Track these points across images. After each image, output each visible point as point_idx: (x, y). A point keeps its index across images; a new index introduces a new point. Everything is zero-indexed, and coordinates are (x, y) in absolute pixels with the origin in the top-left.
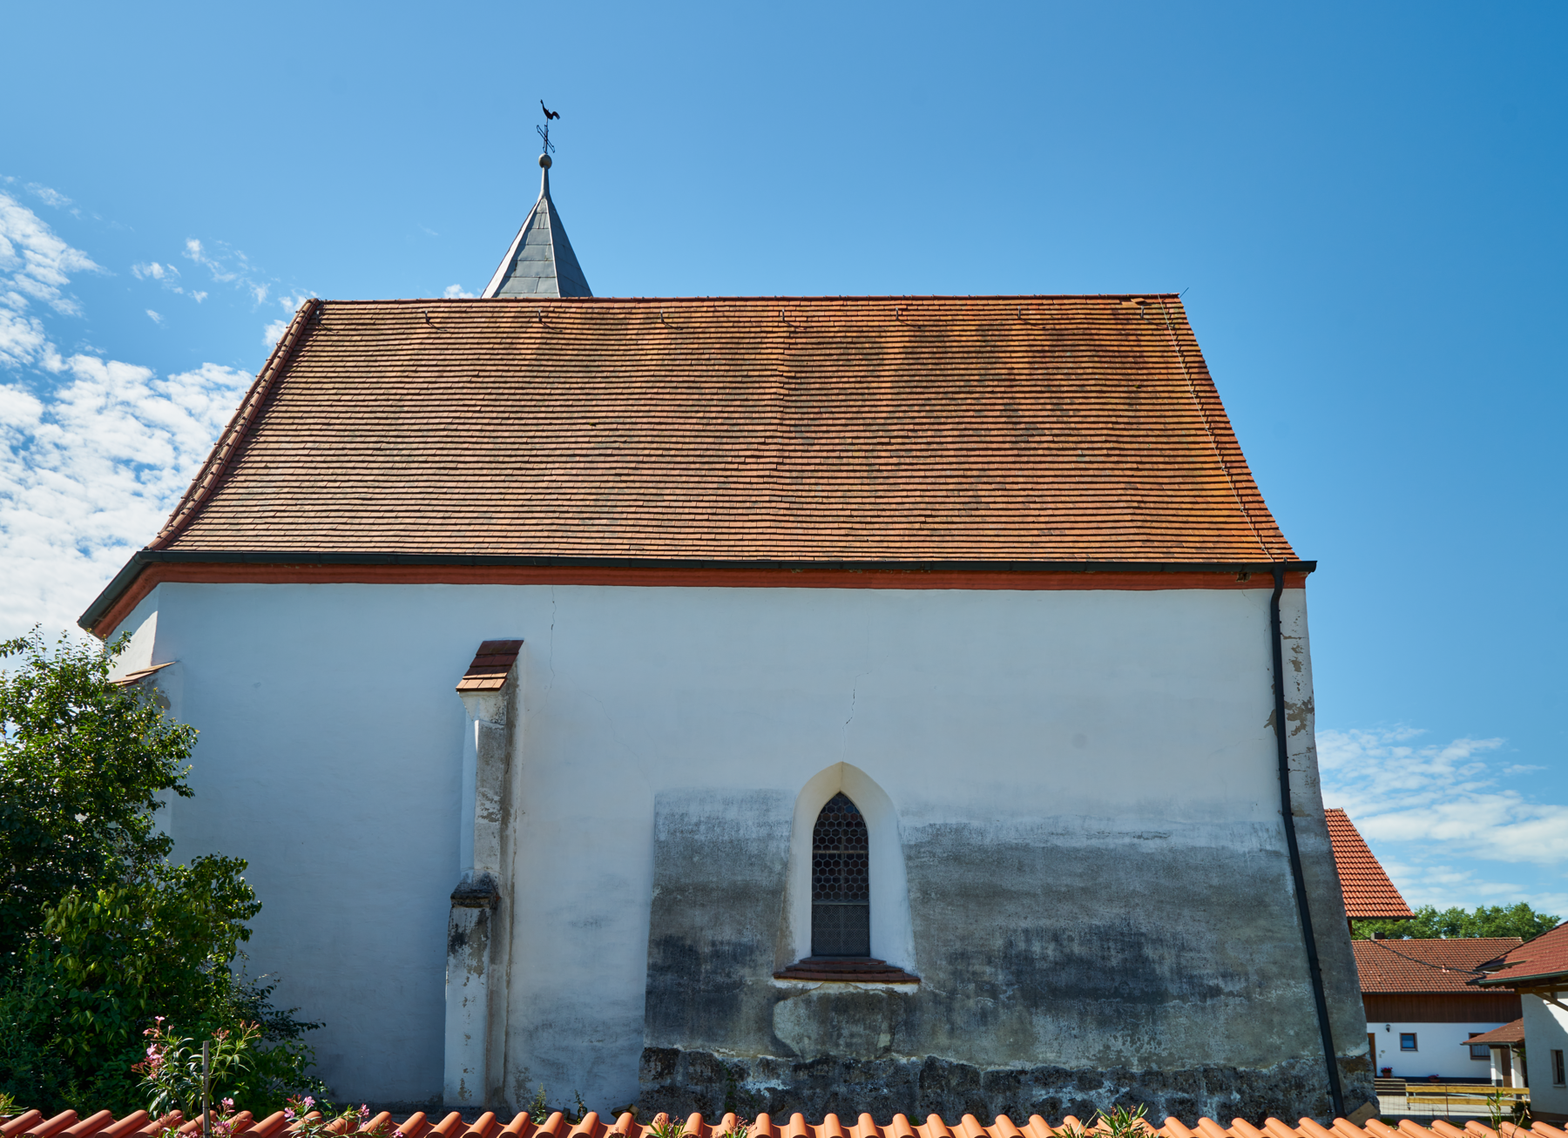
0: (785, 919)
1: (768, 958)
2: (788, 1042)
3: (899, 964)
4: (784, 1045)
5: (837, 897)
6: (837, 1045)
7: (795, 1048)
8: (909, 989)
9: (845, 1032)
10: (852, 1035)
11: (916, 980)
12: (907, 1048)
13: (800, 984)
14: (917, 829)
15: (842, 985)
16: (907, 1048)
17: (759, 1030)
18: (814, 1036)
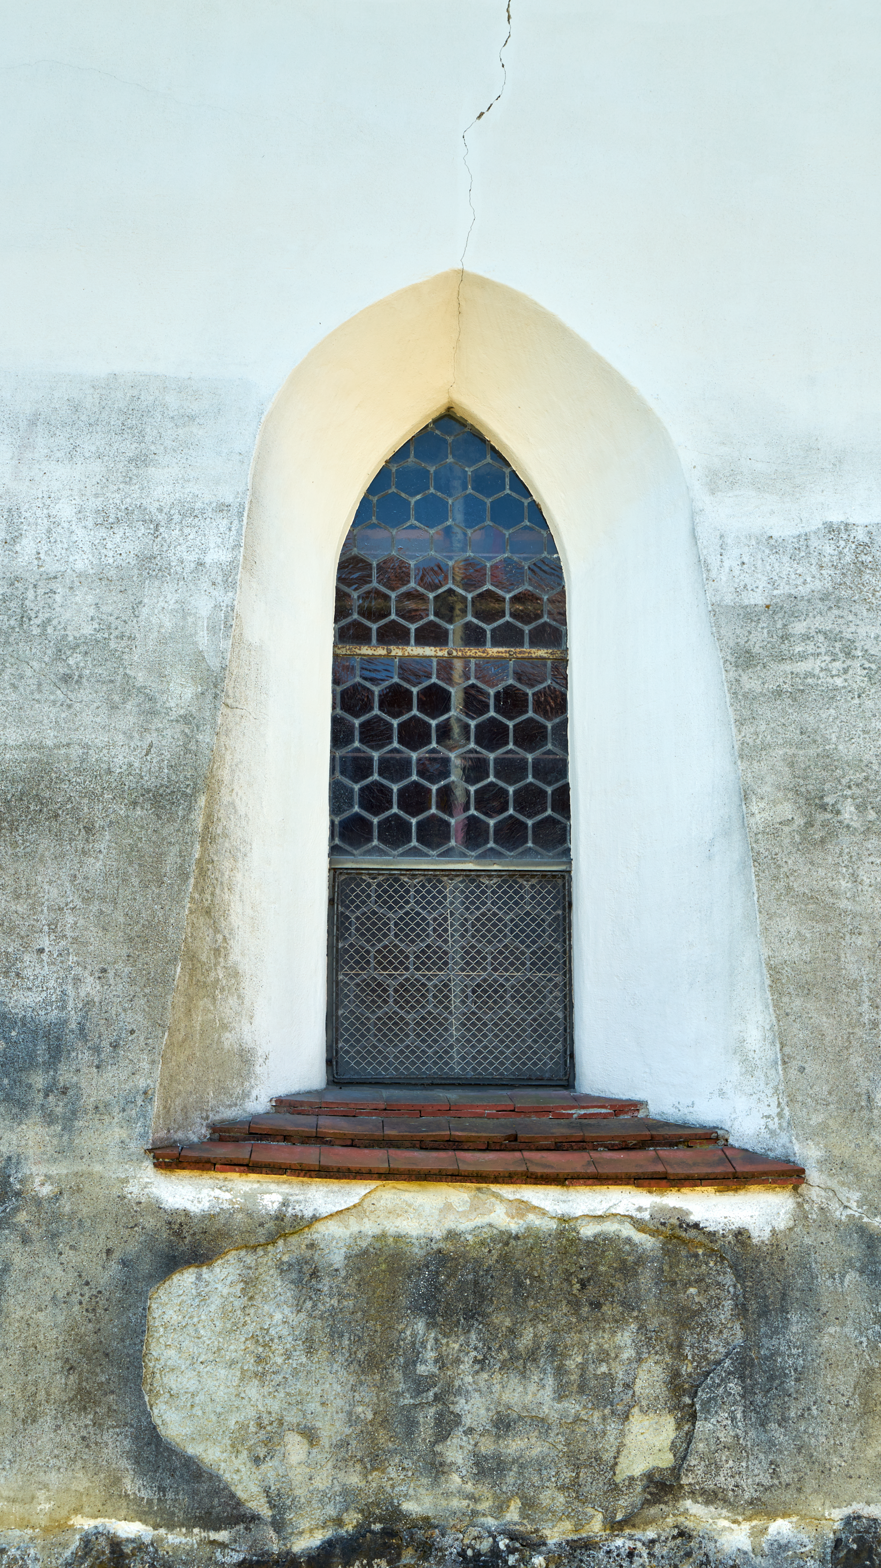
0: (210, 912)
1: (126, 1085)
2: (212, 1454)
3: (705, 1112)
4: (192, 1472)
5: (434, 835)
6: (437, 1469)
7: (247, 1485)
8: (752, 1212)
9: (473, 1409)
10: (503, 1424)
11: (789, 1175)
12: (753, 1476)
13: (270, 1194)
14: (773, 545)
15: (458, 1196)
16: (753, 1476)
17: (83, 1399)
18: (331, 1428)
